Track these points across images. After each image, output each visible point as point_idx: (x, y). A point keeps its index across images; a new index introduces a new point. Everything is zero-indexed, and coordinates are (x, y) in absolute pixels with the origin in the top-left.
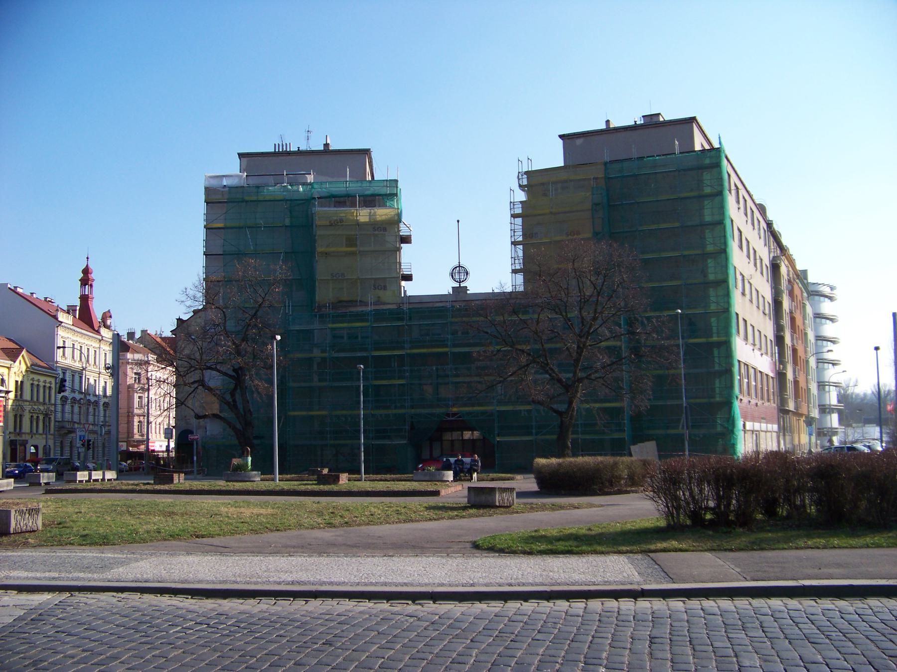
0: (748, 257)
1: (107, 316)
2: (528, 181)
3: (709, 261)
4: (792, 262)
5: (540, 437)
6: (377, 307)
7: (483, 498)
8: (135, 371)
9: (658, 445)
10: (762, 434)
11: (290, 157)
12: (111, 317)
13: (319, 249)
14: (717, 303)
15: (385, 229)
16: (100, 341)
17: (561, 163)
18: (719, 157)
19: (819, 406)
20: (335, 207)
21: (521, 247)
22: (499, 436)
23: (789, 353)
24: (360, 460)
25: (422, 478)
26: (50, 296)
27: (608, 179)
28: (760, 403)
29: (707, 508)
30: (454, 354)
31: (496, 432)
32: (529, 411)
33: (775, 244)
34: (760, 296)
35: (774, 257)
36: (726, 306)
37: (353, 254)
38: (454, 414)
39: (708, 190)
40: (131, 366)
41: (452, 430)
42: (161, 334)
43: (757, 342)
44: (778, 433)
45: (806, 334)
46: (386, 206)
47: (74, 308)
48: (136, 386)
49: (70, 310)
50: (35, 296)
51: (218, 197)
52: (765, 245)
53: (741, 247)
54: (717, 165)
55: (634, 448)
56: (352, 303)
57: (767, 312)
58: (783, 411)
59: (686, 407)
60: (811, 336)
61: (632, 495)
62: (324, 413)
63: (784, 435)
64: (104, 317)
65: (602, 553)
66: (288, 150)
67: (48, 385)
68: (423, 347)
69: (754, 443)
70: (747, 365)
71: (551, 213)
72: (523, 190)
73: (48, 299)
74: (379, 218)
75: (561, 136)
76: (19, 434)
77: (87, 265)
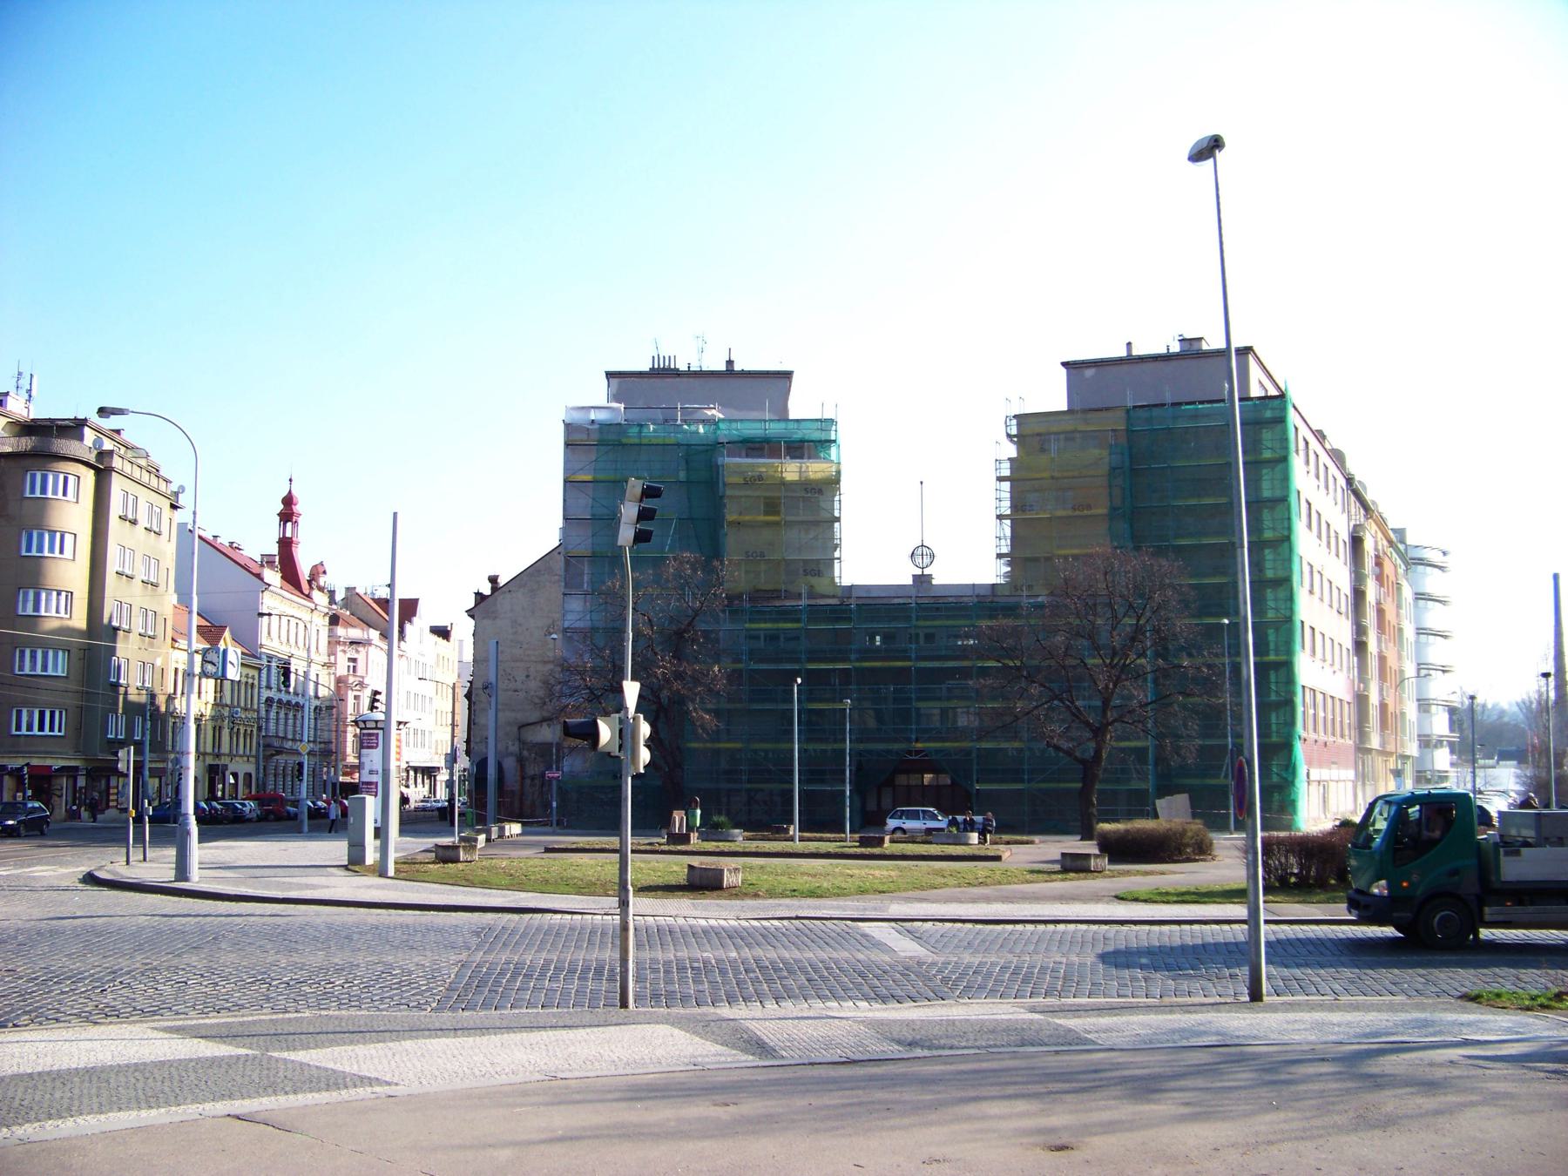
0: (1319, 537)
1: (317, 571)
2: (1018, 429)
3: (1267, 551)
4: (1381, 524)
5: (1034, 785)
6: (812, 602)
7: (1079, 863)
8: (349, 655)
9: (1190, 798)
10: (1332, 785)
11: (678, 379)
12: (325, 572)
13: (731, 516)
14: (1277, 609)
15: (820, 491)
16: (312, 610)
17: (1063, 406)
18: (1284, 409)
19: (1419, 736)
20: (747, 456)
21: (1008, 522)
22: (978, 782)
23: (1373, 664)
24: (844, 817)
25: (944, 840)
26: (238, 541)
27: (1130, 432)
28: (1331, 739)
29: (1292, 874)
30: (920, 670)
31: (975, 777)
32: (1020, 750)
33: (1358, 504)
34: (1333, 587)
35: (1355, 526)
36: (1288, 614)
37: (777, 524)
38: (918, 752)
39: (1267, 455)
40: (342, 648)
41: (907, 772)
42: (374, 594)
43: (1328, 656)
44: (1355, 783)
45: (1400, 630)
46: (820, 458)
47: (271, 559)
48: (351, 679)
49: (268, 561)
50: (219, 540)
51: (578, 437)
52: (1343, 511)
53: (1309, 526)
54: (1281, 420)
55: (1161, 804)
56: (775, 594)
57: (1343, 609)
58: (1362, 749)
59: (1232, 750)
60: (1409, 632)
61: (1201, 863)
62: (738, 745)
63: (1364, 784)
64: (314, 572)
65: (1220, 903)
66: (672, 367)
67: (250, 681)
68: (875, 659)
69: (1321, 796)
70: (1314, 691)
71: (1053, 478)
72: (1011, 441)
73: (235, 545)
74: (812, 476)
75: (1064, 364)
76: (217, 756)
77: (290, 492)
